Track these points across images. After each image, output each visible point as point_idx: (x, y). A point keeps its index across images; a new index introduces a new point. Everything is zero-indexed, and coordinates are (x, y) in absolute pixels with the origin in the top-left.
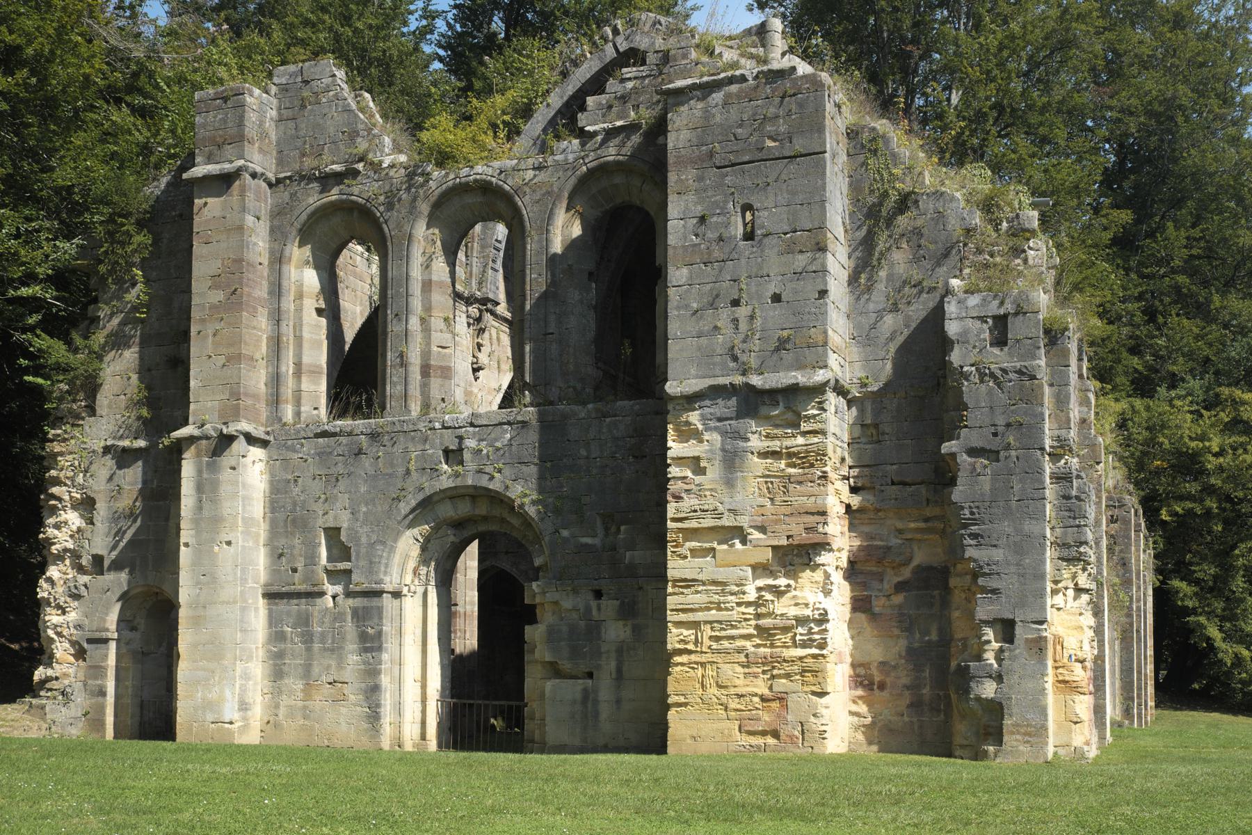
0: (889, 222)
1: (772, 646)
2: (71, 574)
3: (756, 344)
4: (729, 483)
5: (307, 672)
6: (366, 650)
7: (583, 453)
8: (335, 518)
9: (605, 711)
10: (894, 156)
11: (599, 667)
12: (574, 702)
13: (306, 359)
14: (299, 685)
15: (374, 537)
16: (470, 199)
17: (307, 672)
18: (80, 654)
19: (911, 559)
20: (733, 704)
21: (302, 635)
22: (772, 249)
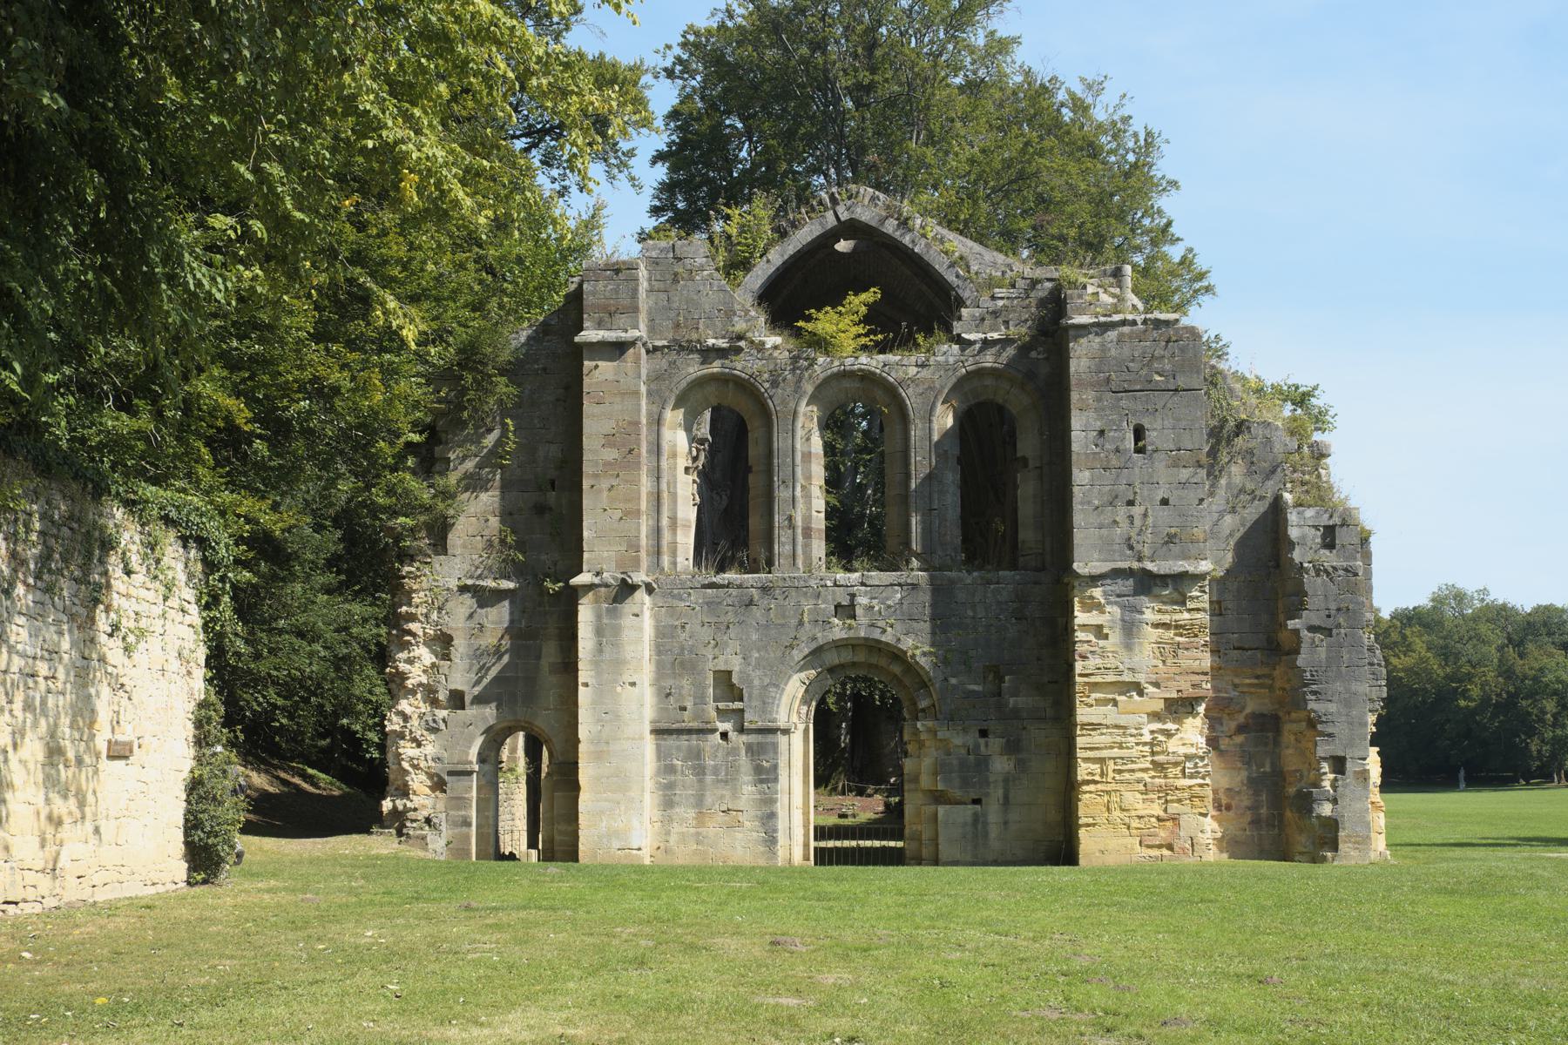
0: (1229, 441)
1: (1166, 777)
2: (425, 708)
3: (1148, 537)
4: (1128, 647)
5: (699, 802)
6: (762, 781)
7: (970, 613)
8: (726, 662)
9: (994, 832)
10: (1231, 390)
11: (987, 795)
12: (965, 824)
13: (680, 515)
14: (691, 813)
15: (767, 681)
16: (847, 384)
17: (699, 802)
18: (439, 785)
19: (1243, 708)
20: (1135, 823)
21: (694, 768)
22: (1160, 463)
